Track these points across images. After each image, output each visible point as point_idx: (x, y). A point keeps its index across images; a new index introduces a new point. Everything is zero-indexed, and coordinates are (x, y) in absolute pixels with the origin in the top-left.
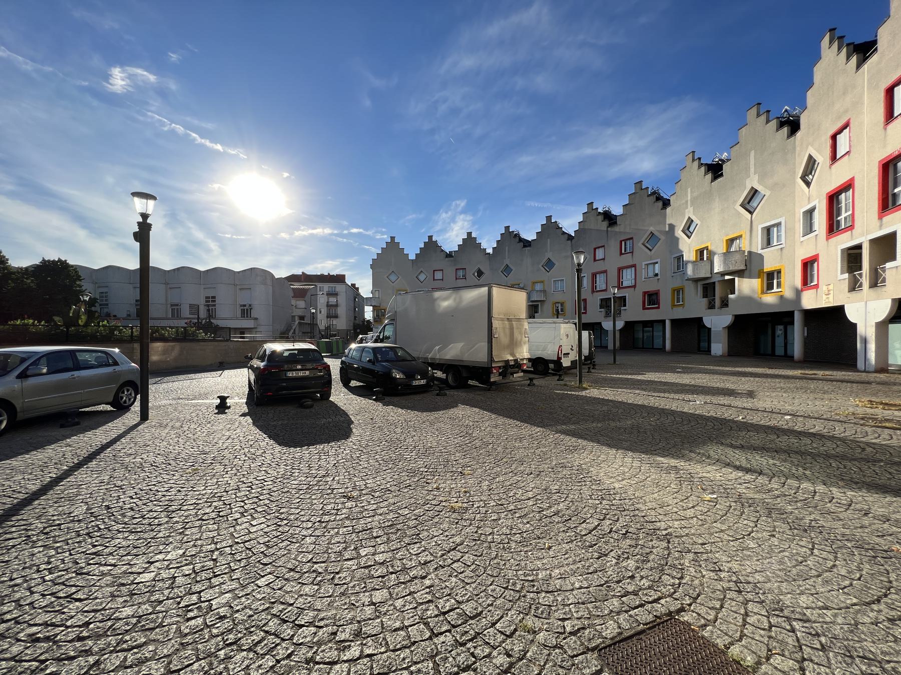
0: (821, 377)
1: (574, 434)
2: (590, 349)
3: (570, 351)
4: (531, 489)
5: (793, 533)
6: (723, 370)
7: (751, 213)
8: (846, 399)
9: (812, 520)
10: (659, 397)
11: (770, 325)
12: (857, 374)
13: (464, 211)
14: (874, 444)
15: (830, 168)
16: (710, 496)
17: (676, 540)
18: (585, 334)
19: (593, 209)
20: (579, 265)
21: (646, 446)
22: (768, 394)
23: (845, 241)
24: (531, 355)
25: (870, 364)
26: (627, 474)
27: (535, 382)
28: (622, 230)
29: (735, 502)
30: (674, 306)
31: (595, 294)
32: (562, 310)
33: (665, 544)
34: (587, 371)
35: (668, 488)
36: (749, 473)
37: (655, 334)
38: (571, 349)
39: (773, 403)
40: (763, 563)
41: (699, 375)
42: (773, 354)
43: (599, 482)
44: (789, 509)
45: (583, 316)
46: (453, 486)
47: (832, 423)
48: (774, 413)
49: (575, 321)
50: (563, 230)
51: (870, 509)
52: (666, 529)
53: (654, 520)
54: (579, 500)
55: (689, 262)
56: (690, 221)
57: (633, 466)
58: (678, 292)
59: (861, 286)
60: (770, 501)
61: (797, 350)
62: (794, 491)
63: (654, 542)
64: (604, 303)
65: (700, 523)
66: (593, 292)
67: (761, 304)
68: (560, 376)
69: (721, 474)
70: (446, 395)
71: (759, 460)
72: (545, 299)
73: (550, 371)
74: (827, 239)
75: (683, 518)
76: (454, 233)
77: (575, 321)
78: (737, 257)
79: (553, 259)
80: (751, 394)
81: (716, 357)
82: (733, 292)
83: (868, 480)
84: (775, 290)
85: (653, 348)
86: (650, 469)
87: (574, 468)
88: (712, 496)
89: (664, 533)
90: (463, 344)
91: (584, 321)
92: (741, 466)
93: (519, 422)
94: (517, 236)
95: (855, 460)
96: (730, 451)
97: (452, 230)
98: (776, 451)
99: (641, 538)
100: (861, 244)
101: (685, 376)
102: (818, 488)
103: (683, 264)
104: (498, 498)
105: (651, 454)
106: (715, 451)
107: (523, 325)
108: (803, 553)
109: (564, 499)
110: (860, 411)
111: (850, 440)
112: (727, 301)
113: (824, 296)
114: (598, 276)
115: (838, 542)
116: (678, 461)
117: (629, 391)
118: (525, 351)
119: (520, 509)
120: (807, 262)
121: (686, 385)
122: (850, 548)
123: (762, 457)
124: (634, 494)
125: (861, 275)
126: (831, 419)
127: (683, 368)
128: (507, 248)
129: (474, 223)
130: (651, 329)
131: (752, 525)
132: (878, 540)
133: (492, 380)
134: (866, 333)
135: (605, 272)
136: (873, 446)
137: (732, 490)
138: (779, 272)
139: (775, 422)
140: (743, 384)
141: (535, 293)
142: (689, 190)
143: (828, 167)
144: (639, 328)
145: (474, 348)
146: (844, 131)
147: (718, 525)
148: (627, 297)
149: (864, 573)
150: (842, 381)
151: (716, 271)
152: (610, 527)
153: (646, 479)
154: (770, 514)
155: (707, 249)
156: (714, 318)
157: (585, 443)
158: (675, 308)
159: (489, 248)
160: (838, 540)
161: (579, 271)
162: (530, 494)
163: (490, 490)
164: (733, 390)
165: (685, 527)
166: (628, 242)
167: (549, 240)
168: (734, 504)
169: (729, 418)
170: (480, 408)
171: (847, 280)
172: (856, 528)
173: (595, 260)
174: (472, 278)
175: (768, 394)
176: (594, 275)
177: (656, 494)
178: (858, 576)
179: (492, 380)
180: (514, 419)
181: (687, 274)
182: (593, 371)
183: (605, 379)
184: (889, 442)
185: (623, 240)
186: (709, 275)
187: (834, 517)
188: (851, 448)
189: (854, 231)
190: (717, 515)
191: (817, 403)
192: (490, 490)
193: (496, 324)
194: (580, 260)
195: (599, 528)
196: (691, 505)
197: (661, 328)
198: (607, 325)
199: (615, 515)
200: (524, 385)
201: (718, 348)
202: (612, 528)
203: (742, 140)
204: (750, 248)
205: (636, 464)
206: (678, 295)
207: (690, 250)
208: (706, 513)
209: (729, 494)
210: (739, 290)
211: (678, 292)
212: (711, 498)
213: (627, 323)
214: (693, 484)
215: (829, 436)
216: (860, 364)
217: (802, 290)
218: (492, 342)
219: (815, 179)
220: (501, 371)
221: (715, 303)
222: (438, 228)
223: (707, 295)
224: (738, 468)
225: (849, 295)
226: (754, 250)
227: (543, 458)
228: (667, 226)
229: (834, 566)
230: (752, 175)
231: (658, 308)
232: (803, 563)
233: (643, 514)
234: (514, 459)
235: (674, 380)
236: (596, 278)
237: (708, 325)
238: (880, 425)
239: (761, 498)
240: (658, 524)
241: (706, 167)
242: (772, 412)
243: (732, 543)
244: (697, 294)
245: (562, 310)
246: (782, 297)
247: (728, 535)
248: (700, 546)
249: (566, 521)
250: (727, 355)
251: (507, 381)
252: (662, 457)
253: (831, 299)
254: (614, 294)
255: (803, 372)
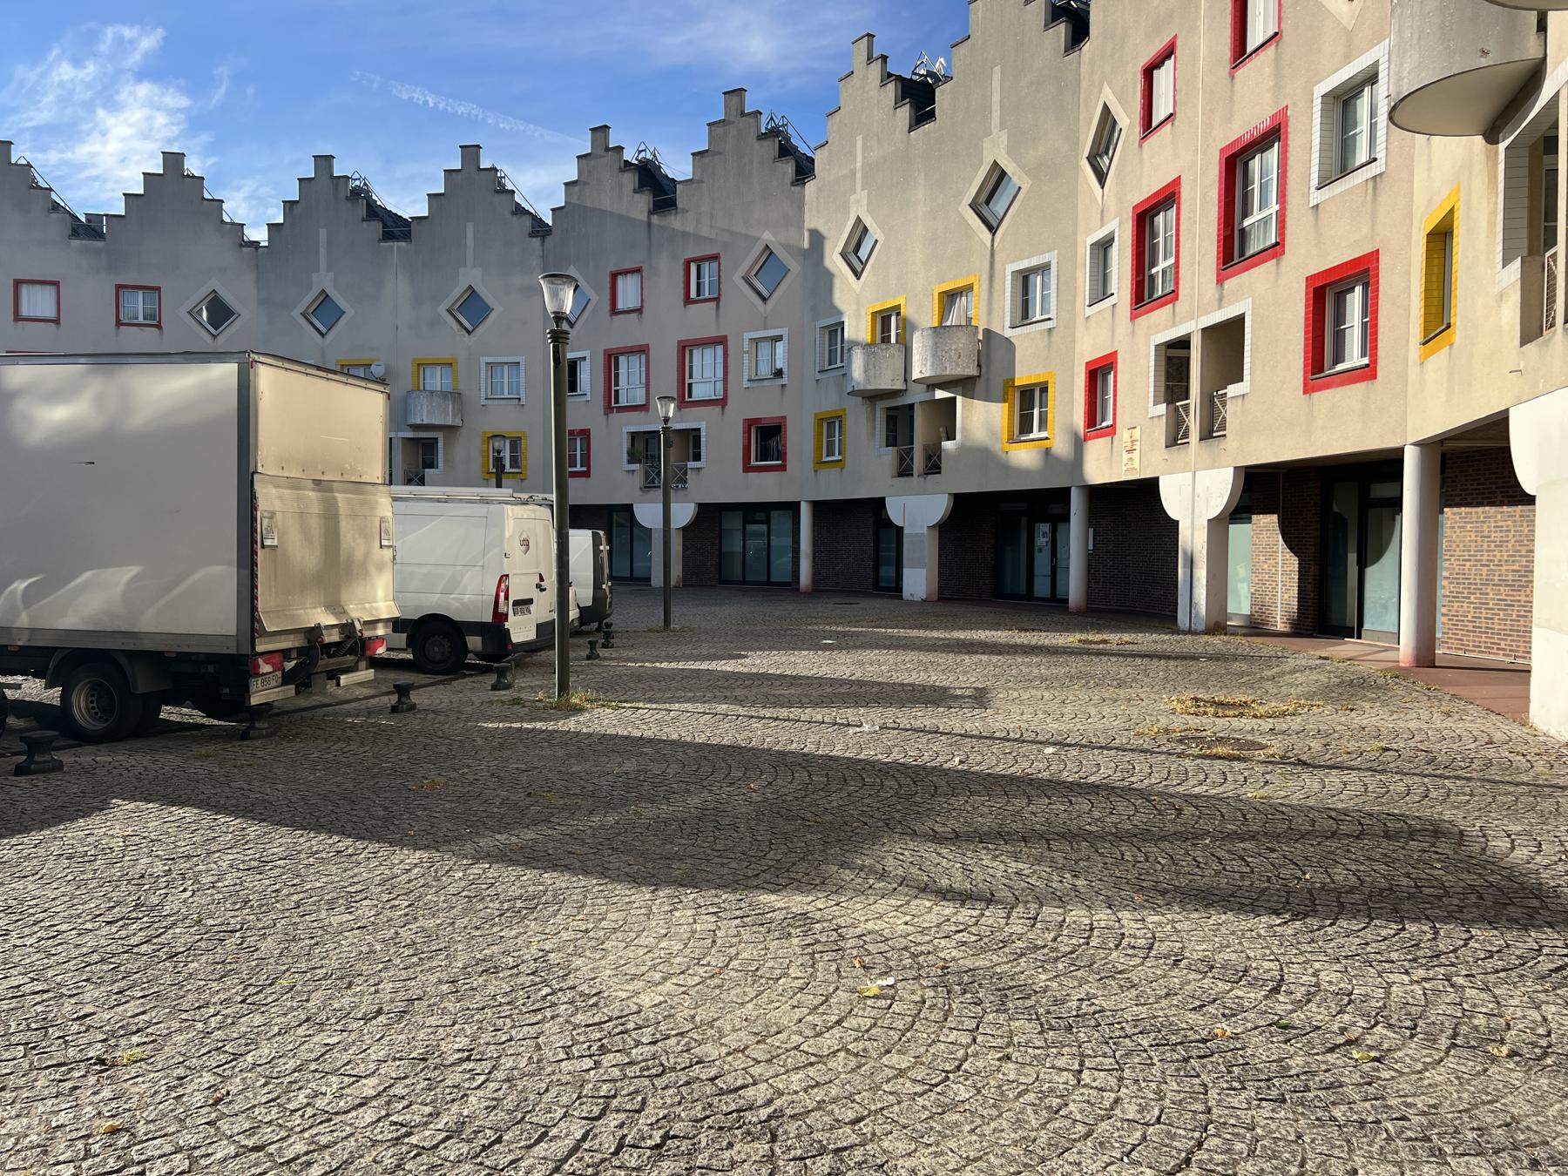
0: (1114, 647)
1: (530, 858)
2: (597, 585)
3: (534, 594)
4: (372, 1066)
5: (1046, 1040)
6: (926, 639)
7: (992, 229)
8: (1157, 697)
9: (1082, 1000)
10: (776, 719)
11: (1024, 521)
12: (1176, 637)
13: (153, 71)
14: (1197, 796)
15: (1140, 146)
16: (880, 982)
17: (792, 1128)
18: (581, 541)
19: (607, 149)
20: (559, 317)
21: (733, 865)
22: (1016, 694)
23: (1163, 326)
24: (400, 607)
25: (1198, 614)
26: (678, 960)
27: (415, 697)
28: (690, 228)
29: (935, 986)
30: (820, 463)
31: (615, 416)
32: (515, 462)
33: (763, 1147)
34: (587, 652)
35: (780, 982)
36: (968, 904)
37: (775, 540)
38: (538, 586)
39: (1024, 717)
40: (983, 1135)
41: (872, 654)
42: (1029, 595)
43: (595, 999)
44: (1041, 981)
45: (573, 483)
46: (63, 1118)
47: (1129, 756)
48: (1024, 741)
49: (548, 496)
50: (517, 198)
51: (1183, 948)
52: (769, 1102)
53: (739, 1083)
54: (532, 1068)
55: (857, 344)
56: (861, 228)
57: (694, 932)
58: (831, 425)
59: (1186, 435)
60: (1006, 968)
61: (1075, 587)
62: (1052, 935)
63: (737, 1147)
64: (640, 446)
65: (853, 1062)
66: (609, 409)
67: (1007, 469)
68: (501, 673)
69: (908, 918)
70: (58, 767)
71: (994, 867)
72: (458, 422)
73: (471, 659)
74: (1133, 317)
75: (813, 1059)
76: (113, 146)
77: (548, 496)
78: (961, 342)
79: (482, 291)
80: (980, 698)
81: (911, 603)
82: (951, 436)
83: (1183, 881)
84: (1035, 434)
85: (768, 583)
86: (739, 934)
87: (523, 968)
88: (885, 983)
89: (764, 1113)
90: (131, 572)
91: (574, 498)
92: (950, 889)
93: (349, 842)
94: (361, 195)
95: (1164, 838)
96: (928, 851)
97: (104, 134)
98: (1024, 839)
99: (703, 1144)
100: (1189, 335)
101: (841, 656)
102: (1097, 917)
103: (842, 348)
104: (247, 1125)
105: (747, 887)
106: (898, 855)
107: (372, 506)
108: (1061, 1087)
109: (483, 1078)
110: (1178, 723)
111: (1160, 794)
112: (939, 457)
113: (1125, 453)
114: (622, 360)
115: (1127, 1040)
116: (810, 898)
117: (700, 707)
118: (380, 593)
119: (327, 1147)
120: (1096, 369)
121: (841, 682)
122: (1145, 1051)
123: (995, 858)
124: (693, 1017)
125: (1186, 408)
126: (1128, 747)
127: (838, 635)
128: (323, 233)
129: (195, 123)
130: (764, 527)
131: (965, 1039)
132: (1193, 1018)
133: (255, 700)
134: (1192, 547)
135: (643, 350)
136: (1195, 802)
137: (930, 957)
138: (1044, 389)
139: (1026, 765)
140: (963, 673)
141: (423, 400)
142: (859, 139)
143: (1137, 144)
144: (734, 523)
145: (180, 589)
146: (1166, 62)
147: (893, 1059)
148: (703, 434)
149: (1167, 1102)
150: (1151, 656)
151: (916, 375)
152: (619, 1133)
153: (727, 965)
154: (1004, 1003)
155: (898, 314)
156: (913, 501)
157: (560, 880)
158: (823, 472)
159: (255, 225)
160: (1127, 1036)
161: (559, 338)
162: (369, 1087)
163: (218, 1101)
164: (946, 689)
165: (817, 1085)
166: (706, 267)
167: (470, 226)
168: (932, 994)
169: (933, 764)
170: (203, 804)
171: (1164, 418)
172: (1158, 999)
173: (614, 311)
174: (183, 325)
175: (1016, 694)
176: (612, 359)
177: (750, 1006)
178: (1156, 1112)
179: (255, 700)
180: (330, 832)
181: (852, 378)
182: (603, 653)
183: (637, 677)
184: (1221, 789)
185: (694, 260)
186: (899, 385)
187: (1122, 983)
188: (1160, 812)
189: (1178, 304)
190: (892, 1033)
191: (1106, 711)
192: (218, 1101)
193: (268, 498)
194: (561, 303)
195: (586, 1146)
196: (834, 1018)
197: (789, 525)
198: (648, 514)
199: (637, 1092)
200: (379, 711)
201: (918, 580)
202: (624, 1136)
203: (975, 30)
204: (989, 322)
205: (705, 923)
206: (830, 434)
207: (858, 310)
208: (867, 1031)
209: (923, 967)
210: (964, 429)
211: (830, 424)
212: (882, 988)
213: (703, 508)
214: (842, 958)
215: (1122, 789)
216: (1182, 619)
217: (1086, 439)
218: (254, 564)
219: (1116, 165)
220: (289, 665)
221: (912, 459)
222: (42, 115)
223: (895, 438)
224: (945, 894)
225: (1166, 454)
226: (996, 328)
227: (422, 952)
228: (806, 234)
229: (1117, 1101)
230: (995, 131)
231: (782, 468)
232: (1061, 1113)
233: (713, 1072)
234: (320, 973)
235: (815, 671)
236: (617, 368)
237: (896, 519)
238: (1209, 751)
239: (988, 964)
240: (750, 1092)
241: (899, 86)
242: (1021, 740)
243: (920, 1101)
244: (873, 435)
245: (515, 462)
246: (1047, 451)
247: (915, 1081)
248: (848, 1130)
249: (484, 1148)
250: (936, 598)
251: (317, 699)
252: (772, 892)
253: (1136, 464)
254: (666, 420)
255: (1084, 637)
